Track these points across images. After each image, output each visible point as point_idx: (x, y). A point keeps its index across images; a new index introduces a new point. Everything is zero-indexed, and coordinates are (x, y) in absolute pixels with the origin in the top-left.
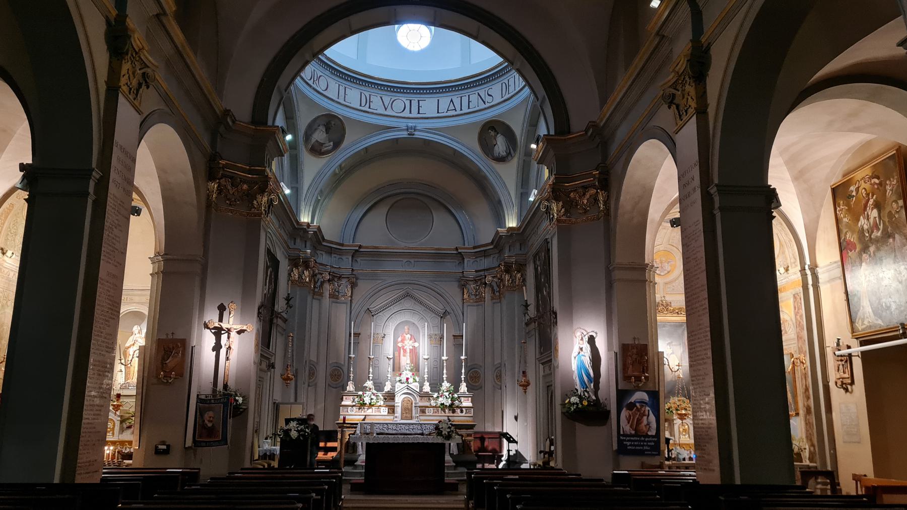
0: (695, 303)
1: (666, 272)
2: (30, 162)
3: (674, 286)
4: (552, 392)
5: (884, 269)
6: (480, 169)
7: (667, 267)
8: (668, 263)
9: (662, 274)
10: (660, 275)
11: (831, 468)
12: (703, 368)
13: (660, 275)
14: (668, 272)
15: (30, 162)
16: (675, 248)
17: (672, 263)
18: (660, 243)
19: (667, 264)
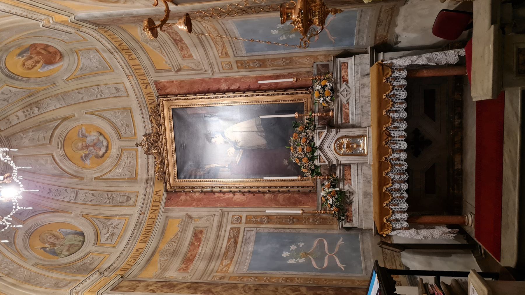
0: (399, 136)
1: (101, 138)
2: (441, 277)
3: (122, 125)
4: (140, 69)
5: (244, 133)
6: (111, 15)
7: (93, 138)
8: (87, 137)
9: (105, 143)
10: (107, 147)
11: (482, 269)
12: (301, 138)
13: (107, 147)
14: (101, 134)
15: (441, 277)
16: (57, 132)
17: (84, 131)
18: (50, 159)
19: (88, 139)
